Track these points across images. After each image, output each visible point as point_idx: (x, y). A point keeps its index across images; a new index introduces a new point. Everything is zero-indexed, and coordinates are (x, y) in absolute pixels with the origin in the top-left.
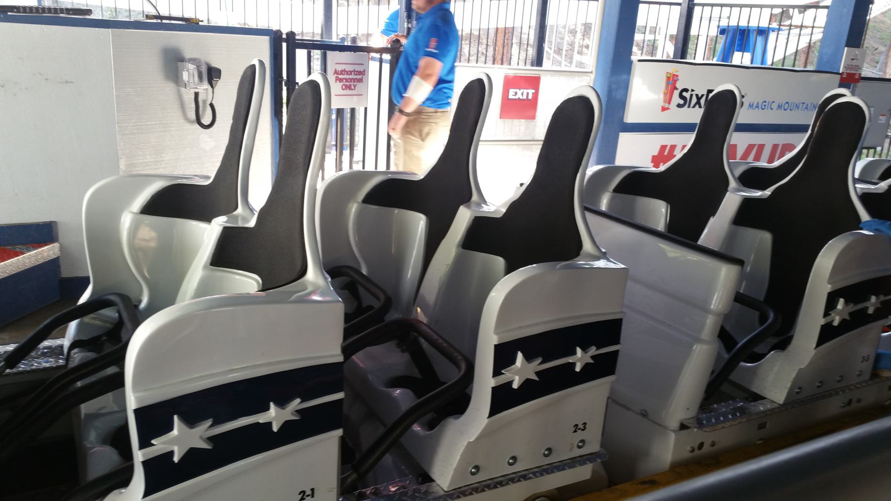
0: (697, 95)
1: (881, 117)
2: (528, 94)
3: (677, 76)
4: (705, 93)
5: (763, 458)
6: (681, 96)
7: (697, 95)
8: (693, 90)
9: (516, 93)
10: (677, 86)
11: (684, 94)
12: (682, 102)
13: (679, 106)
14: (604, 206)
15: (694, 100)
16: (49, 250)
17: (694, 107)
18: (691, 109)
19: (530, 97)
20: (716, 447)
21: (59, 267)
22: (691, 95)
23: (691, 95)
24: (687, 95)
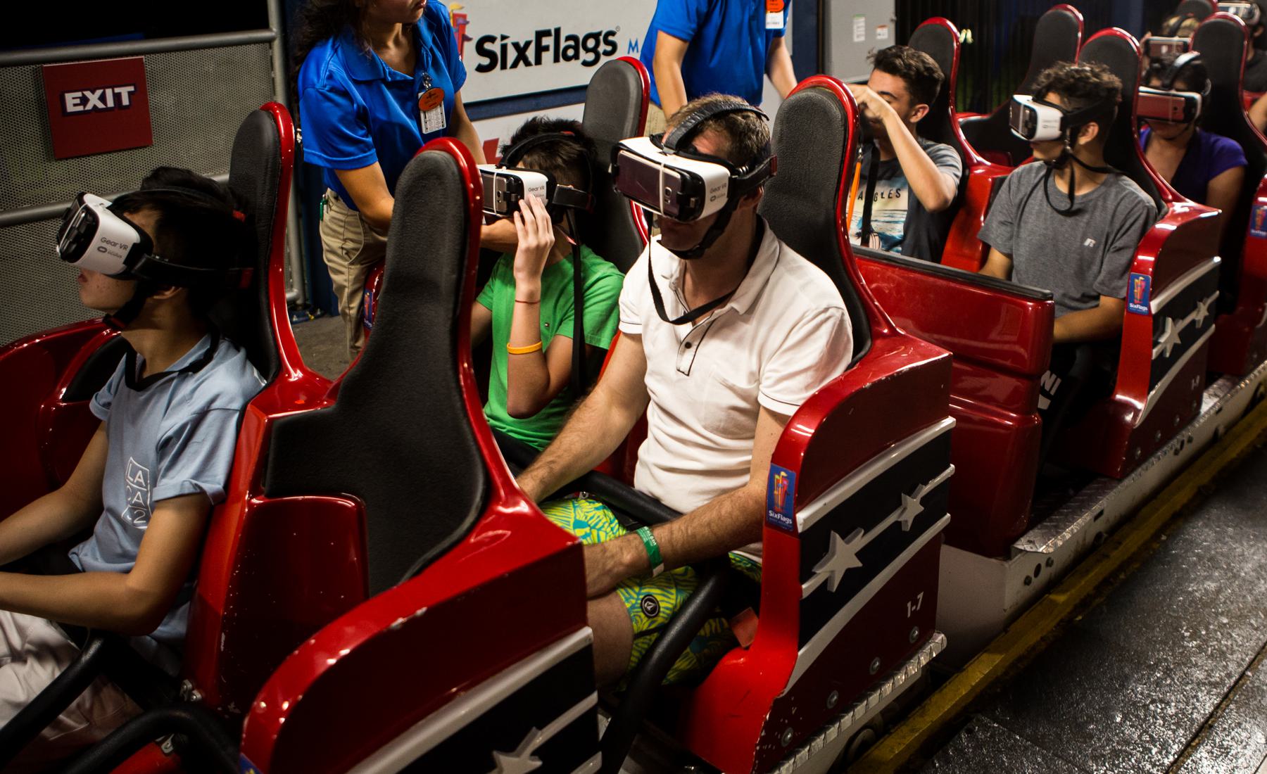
0: (516, 45)
1: (879, 31)
2: (117, 97)
3: (464, 16)
4: (532, 37)
5: (881, 471)
6: (480, 50)
7: (516, 45)
8: (503, 38)
9: (84, 101)
10: (468, 32)
11: (488, 46)
12: (486, 61)
13: (481, 69)
14: (914, 120)
15: (512, 54)
16: (673, 75)
17: (515, 65)
18: (508, 71)
19: (125, 101)
20: (1194, 442)
21: (1120, 336)
22: (504, 48)
23: (504, 48)
24: (495, 47)
